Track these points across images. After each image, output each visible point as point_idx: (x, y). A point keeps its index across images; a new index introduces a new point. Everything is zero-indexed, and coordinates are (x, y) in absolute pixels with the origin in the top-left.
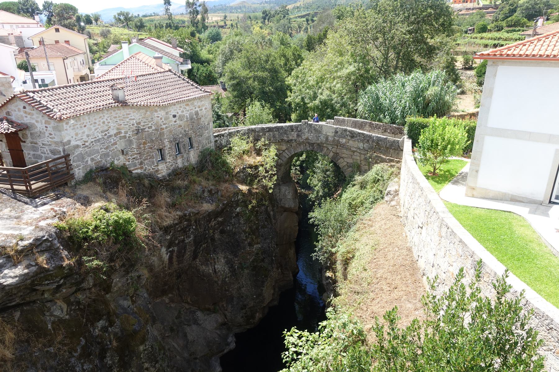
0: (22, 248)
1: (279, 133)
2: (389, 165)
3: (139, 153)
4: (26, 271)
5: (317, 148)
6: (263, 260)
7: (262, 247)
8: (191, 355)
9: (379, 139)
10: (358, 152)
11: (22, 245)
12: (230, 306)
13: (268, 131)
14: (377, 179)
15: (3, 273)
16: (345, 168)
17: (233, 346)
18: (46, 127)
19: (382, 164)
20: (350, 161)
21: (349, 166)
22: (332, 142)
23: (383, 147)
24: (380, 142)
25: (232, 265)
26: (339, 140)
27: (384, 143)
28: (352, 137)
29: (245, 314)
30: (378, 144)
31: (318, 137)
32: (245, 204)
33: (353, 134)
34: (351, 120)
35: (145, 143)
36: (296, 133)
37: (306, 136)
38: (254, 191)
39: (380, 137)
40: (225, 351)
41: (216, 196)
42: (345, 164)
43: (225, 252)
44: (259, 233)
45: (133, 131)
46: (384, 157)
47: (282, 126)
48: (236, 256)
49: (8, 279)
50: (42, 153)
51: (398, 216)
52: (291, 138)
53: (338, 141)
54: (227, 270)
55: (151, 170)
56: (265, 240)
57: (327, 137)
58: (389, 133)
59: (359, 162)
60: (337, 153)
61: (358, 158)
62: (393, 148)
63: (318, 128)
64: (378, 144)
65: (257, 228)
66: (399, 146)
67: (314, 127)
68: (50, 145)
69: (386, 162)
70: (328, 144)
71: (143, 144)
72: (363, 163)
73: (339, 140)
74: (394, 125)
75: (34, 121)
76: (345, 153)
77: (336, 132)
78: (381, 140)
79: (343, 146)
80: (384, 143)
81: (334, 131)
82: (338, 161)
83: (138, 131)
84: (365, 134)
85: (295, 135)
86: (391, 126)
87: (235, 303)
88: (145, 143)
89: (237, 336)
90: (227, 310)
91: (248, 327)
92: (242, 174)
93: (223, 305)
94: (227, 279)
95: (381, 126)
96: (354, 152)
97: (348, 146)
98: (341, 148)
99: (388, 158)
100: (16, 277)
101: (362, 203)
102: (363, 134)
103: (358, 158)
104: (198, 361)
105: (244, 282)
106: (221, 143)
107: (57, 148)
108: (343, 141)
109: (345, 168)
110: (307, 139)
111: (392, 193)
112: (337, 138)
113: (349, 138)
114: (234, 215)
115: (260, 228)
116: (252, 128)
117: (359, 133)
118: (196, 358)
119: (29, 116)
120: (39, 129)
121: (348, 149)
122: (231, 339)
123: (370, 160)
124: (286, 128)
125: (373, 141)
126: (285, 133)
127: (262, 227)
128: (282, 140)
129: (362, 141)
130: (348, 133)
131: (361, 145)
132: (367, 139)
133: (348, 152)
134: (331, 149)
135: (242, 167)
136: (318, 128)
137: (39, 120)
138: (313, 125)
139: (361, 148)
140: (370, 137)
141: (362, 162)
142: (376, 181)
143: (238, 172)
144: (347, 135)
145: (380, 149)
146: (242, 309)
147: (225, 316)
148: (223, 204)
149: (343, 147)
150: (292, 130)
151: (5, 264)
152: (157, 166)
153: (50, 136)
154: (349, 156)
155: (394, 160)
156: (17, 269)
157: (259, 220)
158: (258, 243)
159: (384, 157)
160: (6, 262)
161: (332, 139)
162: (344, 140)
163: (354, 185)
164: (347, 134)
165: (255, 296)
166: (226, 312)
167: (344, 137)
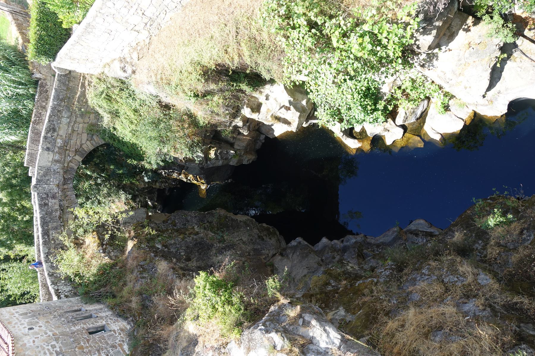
0: (286, 340)
2: (88, 88)
3: (98, 351)
4: (314, 322)
5: (70, 174)
6: (210, 223)
7: (196, 224)
8: (321, 265)
9: (57, 98)
10: (74, 125)
11: (282, 342)
12: (263, 252)
13: (48, 236)
14: (106, 97)
15: (327, 346)
16: (94, 143)
17: (299, 239)
19: (87, 96)
21: (91, 138)
22: (62, 155)
23: (66, 94)
24: (61, 97)
25: (222, 248)
26: (59, 147)
27: (62, 92)
28: (54, 130)
29: (267, 236)
30: (62, 100)
31: (55, 172)
32: (150, 239)
33: (50, 130)
34: (29, 146)
35: (82, 348)
36: (50, 200)
38: (133, 233)
39: (54, 97)
40: (306, 243)
41: (146, 267)
42: (88, 143)
43: (211, 256)
44: (182, 228)
46: (79, 93)
48: (212, 245)
49: (332, 338)
51: (149, 43)
52: (57, 207)
53: (60, 148)
54: (229, 253)
55: (122, 335)
56: (188, 221)
57: (55, 161)
58: (46, 104)
59: (86, 125)
60: (76, 151)
61: (81, 125)
62: (67, 83)
63: (42, 172)
64: (62, 100)
65: (177, 231)
66: (65, 75)
67: (41, 177)
69: (85, 91)
70: (65, 160)
71: (84, 349)
72: (87, 120)
73: (59, 147)
74: (36, 97)
76: (75, 142)
77: (48, 149)
78: (58, 96)
79: (66, 143)
80: (62, 92)
81: (47, 152)
82: (85, 151)
84: (50, 115)
85: (53, 201)
86: (38, 101)
87: (259, 247)
88: (82, 348)
89: (288, 241)
90: (268, 255)
91: (278, 233)
92: (112, 254)
93: (264, 259)
94: (238, 253)
96: (73, 131)
97: (66, 137)
98: (69, 146)
99: (80, 89)
100: (325, 330)
101: (136, 111)
102: (50, 116)
103: (81, 125)
104: (324, 258)
105: (237, 239)
106: (69, 291)
108: (59, 142)
109: (94, 143)
110: (58, 186)
111: (122, 65)
112: (56, 150)
113: (55, 134)
114: (166, 249)
115: (175, 228)
116: (45, 258)
117: (49, 121)
118: (322, 260)
121: (70, 137)
122: (293, 243)
123: (83, 110)
124: (44, 213)
125: (60, 105)
126: (51, 213)
127: (175, 225)
128: (60, 217)
129: (59, 118)
130: (49, 135)
131: (65, 121)
132: (56, 112)
133: (74, 138)
134: (71, 158)
135: (103, 255)
136: (42, 172)
138: (39, 178)
139: (68, 120)
140: (53, 109)
141: (86, 121)
142: (109, 98)
143: (110, 258)
144: (52, 136)
145: (69, 98)
146: (263, 239)
147: (274, 255)
148: (155, 256)
149: (68, 143)
150: (46, 204)
151: (314, 352)
152: (114, 331)
154: (78, 137)
155: (82, 83)
156: (315, 335)
157: (167, 229)
158: (193, 228)
159: (79, 93)
160: (311, 352)
161: (57, 155)
163: (115, 129)
164: (50, 136)
166: (270, 255)
167: (55, 140)
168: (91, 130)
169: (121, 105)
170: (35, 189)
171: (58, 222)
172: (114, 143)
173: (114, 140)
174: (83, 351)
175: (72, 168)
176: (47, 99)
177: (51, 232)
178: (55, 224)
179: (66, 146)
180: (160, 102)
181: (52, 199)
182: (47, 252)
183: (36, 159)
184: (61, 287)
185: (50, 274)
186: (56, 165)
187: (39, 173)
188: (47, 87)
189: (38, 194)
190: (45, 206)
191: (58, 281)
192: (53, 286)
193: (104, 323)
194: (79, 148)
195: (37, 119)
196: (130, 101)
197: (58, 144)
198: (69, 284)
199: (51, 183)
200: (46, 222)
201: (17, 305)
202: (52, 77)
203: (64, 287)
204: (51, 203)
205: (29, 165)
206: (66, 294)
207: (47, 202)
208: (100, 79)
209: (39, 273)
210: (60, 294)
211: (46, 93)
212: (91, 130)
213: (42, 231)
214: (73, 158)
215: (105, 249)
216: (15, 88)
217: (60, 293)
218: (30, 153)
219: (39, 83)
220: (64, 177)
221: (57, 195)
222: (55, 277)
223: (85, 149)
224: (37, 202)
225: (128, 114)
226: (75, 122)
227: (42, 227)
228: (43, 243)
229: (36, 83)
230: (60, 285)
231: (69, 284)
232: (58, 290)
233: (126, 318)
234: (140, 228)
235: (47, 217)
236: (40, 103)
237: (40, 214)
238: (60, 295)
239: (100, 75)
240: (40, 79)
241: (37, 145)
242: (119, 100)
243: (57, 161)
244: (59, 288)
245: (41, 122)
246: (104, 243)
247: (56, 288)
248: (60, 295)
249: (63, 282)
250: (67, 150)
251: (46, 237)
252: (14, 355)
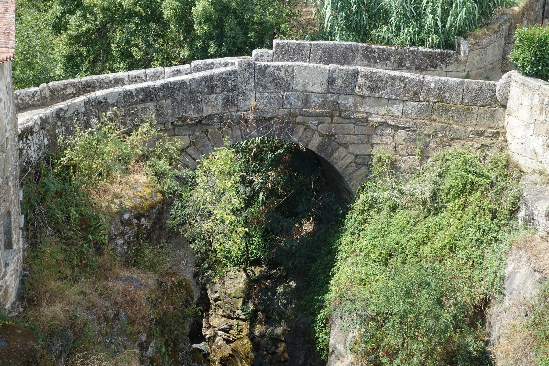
1: (174, 100)
9: (442, 88)
13: (143, 101)
16: (350, 170)
20: (361, 150)
26: (336, 101)
27: (458, 95)
30: (441, 99)
33: (376, 81)
34: (318, 45)
36: (222, 96)
37: (253, 103)
42: (351, 158)
47: (183, 82)
52: (208, 111)
53: (335, 103)
57: (307, 97)
60: (331, 135)
62: (480, 103)
63: (282, 74)
66: (493, 98)
73: (336, 101)
74: (421, 49)
77: (331, 81)
81: (325, 81)
82: (332, 154)
84: (407, 78)
85: (220, 102)
95: (391, 53)
98: (341, 120)
101: (453, 248)
102: (402, 79)
103: (389, 140)
108: (348, 101)
112: (331, 97)
116: (96, 98)
117: (393, 78)
126: (192, 101)
128: (184, 119)
131: (397, 109)
133: (359, 129)
134: (314, 128)
140: (421, 84)
141: (399, 148)
145: (447, 111)
150: (212, 89)
154: (362, 137)
162: (351, 100)
167: (352, 92)
168: (380, 160)
169: (459, 215)
170: (244, 66)
171: (173, 116)
172: (357, 212)
173: (363, 212)
175: (293, 131)
176: (419, 69)
177: (151, 105)
178: (170, 111)
179: (340, 116)
180: (486, 302)
181: (223, 100)
182: (109, 101)
183: (292, 60)
184: (36, 140)
185: (62, 114)
186: (299, 100)
187: (280, 70)
188: (443, 66)
189: (234, 72)
190: (208, 87)
191: (48, 130)
192: (39, 122)
194: (338, 141)
195: (376, 55)
196: (473, 234)
197: (345, 99)
198: (41, 155)
199: (258, 95)
200: (173, 94)
201: (173, 66)
202: (464, 74)
203: (36, 146)
204: (216, 99)
205: (276, 49)
206: (24, 151)
207: (218, 90)
208: (507, 166)
209: (36, 88)
210: (25, 139)
211: (430, 65)
212: (380, 160)
213: (154, 88)
214: (314, 131)
215: (131, 224)
216: (434, 12)
217: (27, 138)
218: (303, 47)
219: (449, 51)
220: (273, 117)
221: (234, 109)
222: (56, 123)
223: (336, 154)
224: (216, 71)
225: (441, 235)
226: (395, 127)
227: (163, 87)
228: (127, 91)
229: (448, 45)
230: (40, 136)
231: (41, 155)
232: (32, 133)
233: (20, 297)
234: (184, 296)
235: (184, 93)
236: (409, 56)
237: (190, 80)
238: (22, 139)
239: (516, 166)
240: (459, 52)
241: (320, 59)
242: (470, 209)
243: (307, 102)
244: (35, 135)
245: (370, 62)
246: (143, 219)
247: (36, 129)
248: (22, 139)
249: (46, 142)
250: (332, 117)
251: (140, 97)
252: (1, 63)
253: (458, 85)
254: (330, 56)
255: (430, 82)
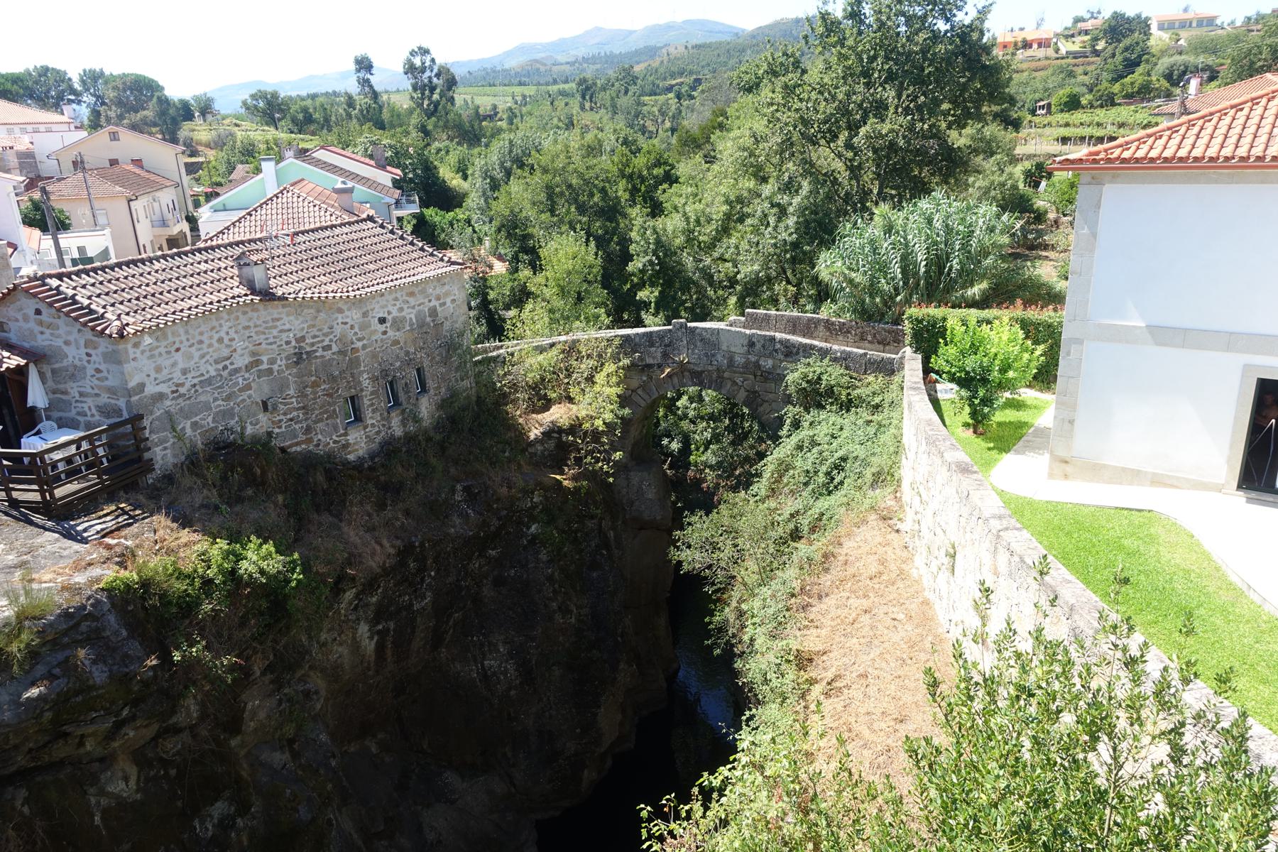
18: (88, 355)
26: (757, 362)
33: (787, 347)
34: (783, 316)
36: (660, 350)
45: (288, 358)
50: (79, 414)
53: (757, 365)
58: (869, 342)
67: (700, 335)
68: (97, 395)
70: (735, 372)
73: (757, 362)
75: (59, 342)
77: (751, 344)
81: (746, 342)
83: (299, 358)
85: (659, 355)
94: (513, 692)
107: (113, 402)
112: (753, 359)
119: (48, 332)
120: (70, 359)
130: (778, 346)
134: (740, 384)
137: (71, 338)
152: (346, 434)
153: (98, 375)
161: (743, 360)
165: (578, 731)
167: (770, 356)
174: (307, 386)
193: (370, 422)
253: (861, 355)
254: (794, 326)
255: (836, 352)
